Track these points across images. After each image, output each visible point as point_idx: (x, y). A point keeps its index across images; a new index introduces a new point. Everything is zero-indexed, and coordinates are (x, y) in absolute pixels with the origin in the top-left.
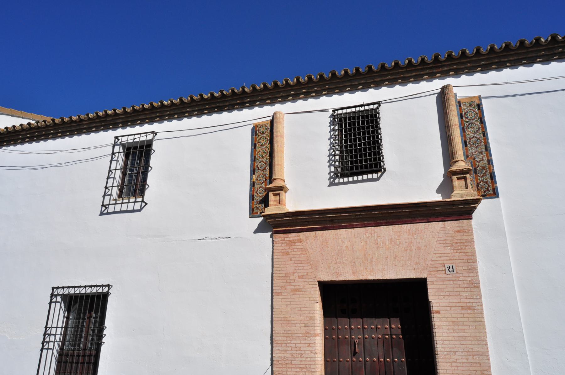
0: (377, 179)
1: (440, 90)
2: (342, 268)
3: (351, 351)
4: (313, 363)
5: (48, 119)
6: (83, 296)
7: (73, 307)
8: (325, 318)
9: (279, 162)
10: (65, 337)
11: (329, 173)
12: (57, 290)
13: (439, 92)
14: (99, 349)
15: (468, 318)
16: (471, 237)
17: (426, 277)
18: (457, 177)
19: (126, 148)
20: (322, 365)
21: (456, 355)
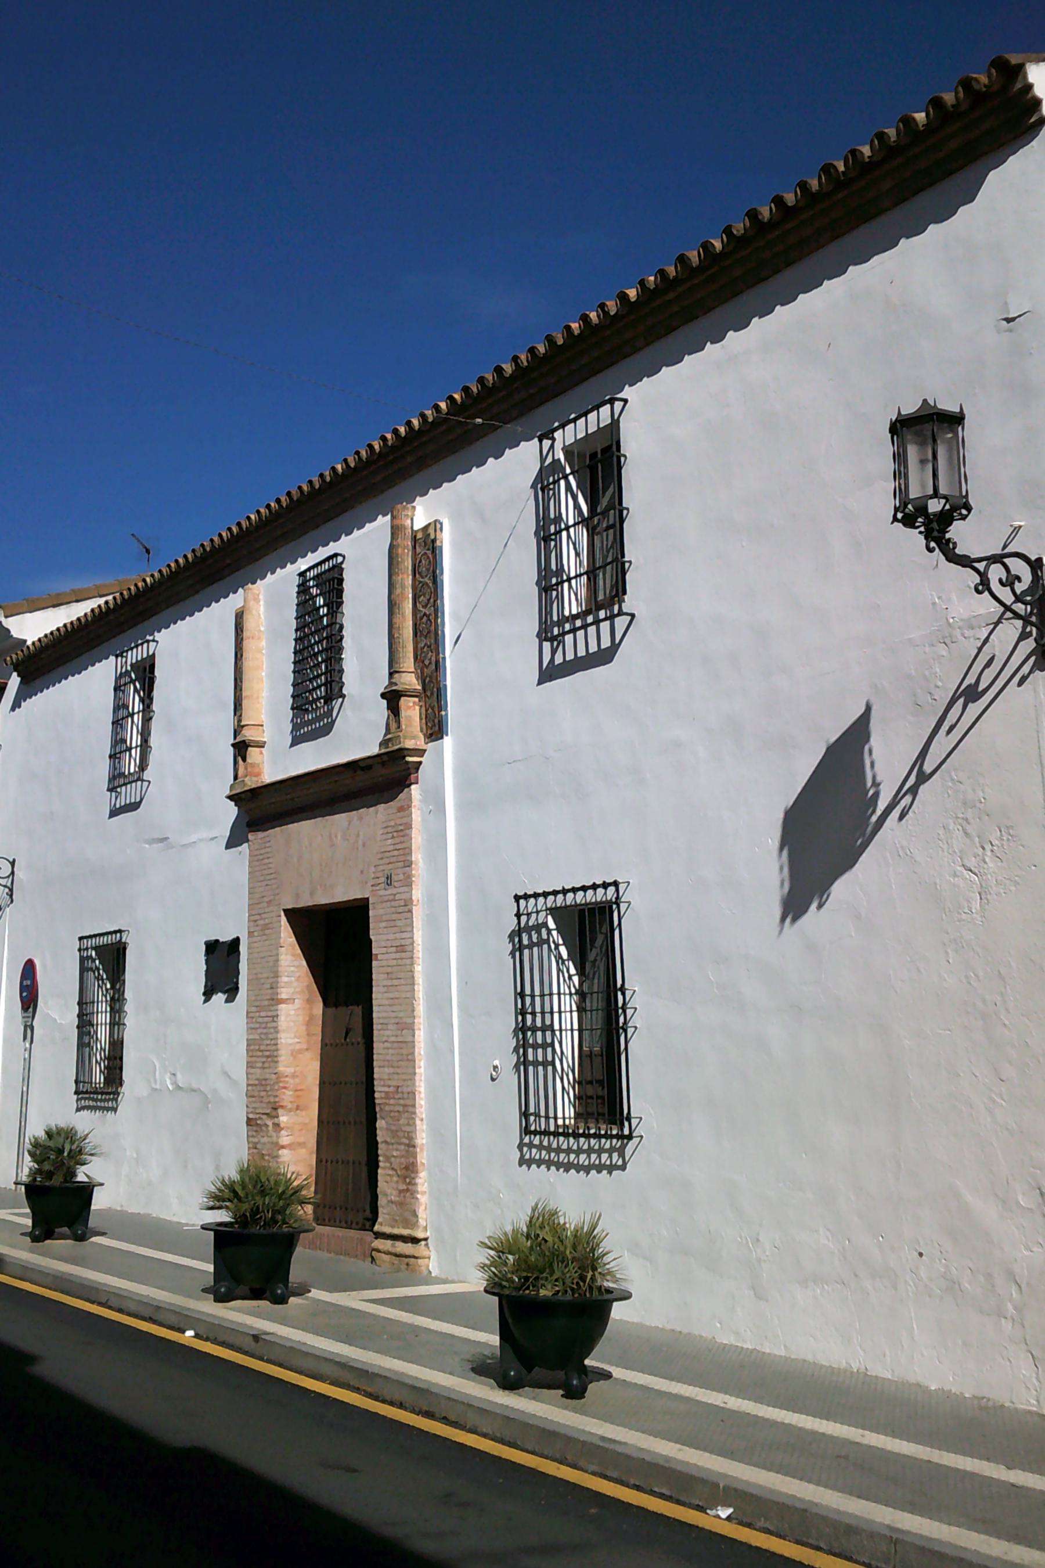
0: (604, 657)
1: (933, 404)
2: (398, 1087)
3: (39, 1285)
4: (274, 1048)
5: (110, 598)
6: (584, 910)
7: (604, 493)
8: (331, 1010)
9: (1026, 609)
10: (326, 1359)
11: (515, 1048)
12: (566, 1142)
13: (19, 679)
14: (716, 1485)
15: (1002, 609)
16: (251, 885)
17: (366, 896)
18: (237, 941)
19: (576, 454)
20: (361, 819)
21: (372, 1230)
